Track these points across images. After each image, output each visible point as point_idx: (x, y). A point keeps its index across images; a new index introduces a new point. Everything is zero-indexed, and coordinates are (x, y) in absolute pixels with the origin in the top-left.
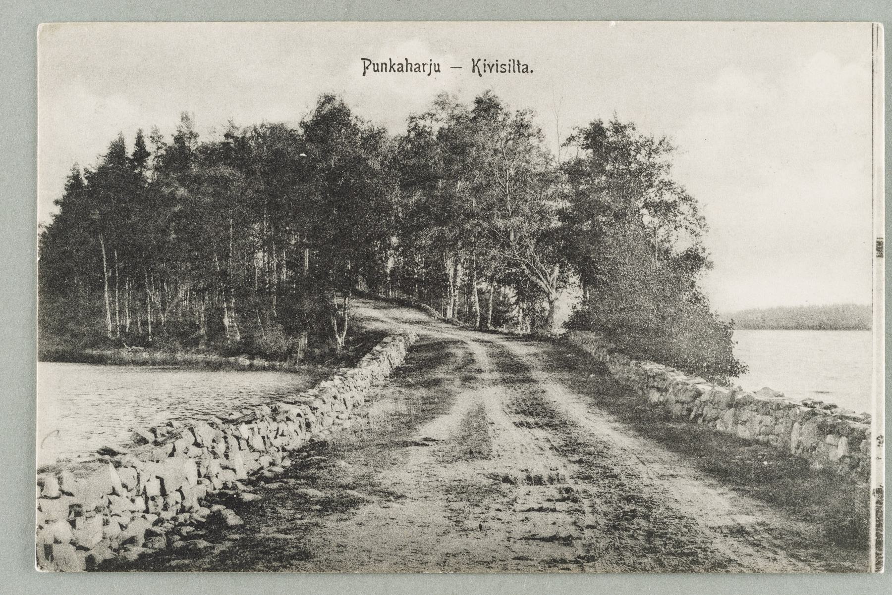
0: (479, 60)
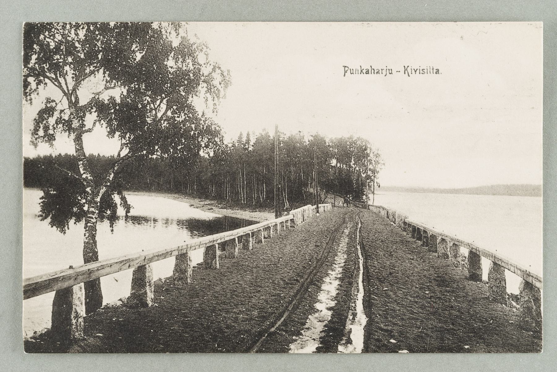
0: (408, 66)
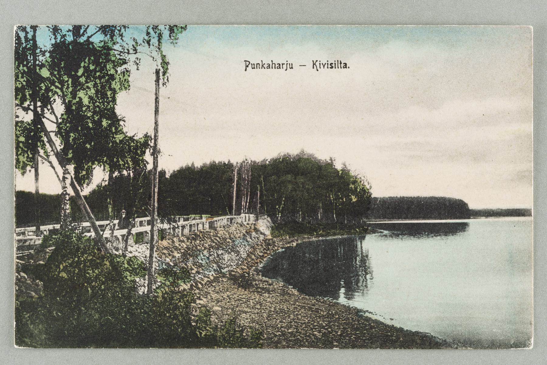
0: (317, 61)
